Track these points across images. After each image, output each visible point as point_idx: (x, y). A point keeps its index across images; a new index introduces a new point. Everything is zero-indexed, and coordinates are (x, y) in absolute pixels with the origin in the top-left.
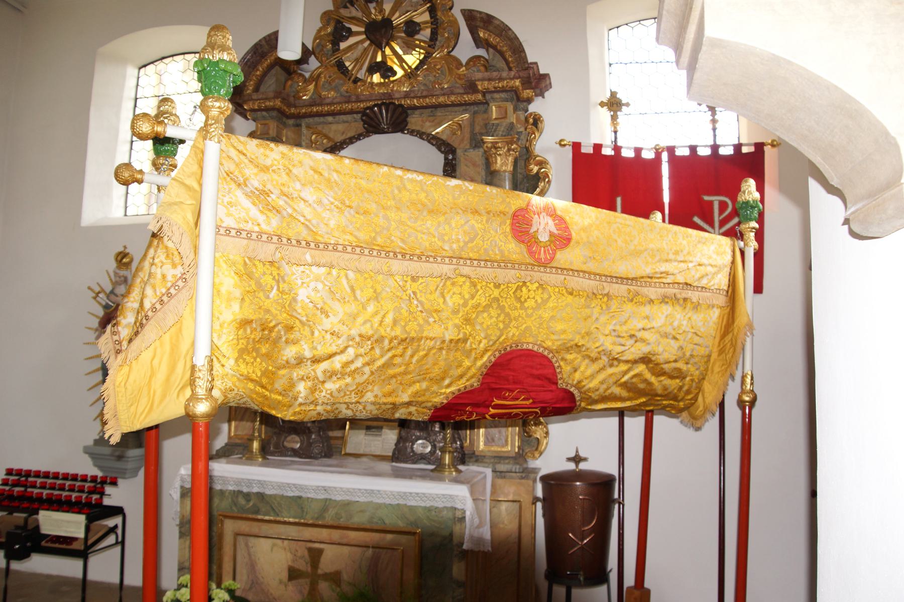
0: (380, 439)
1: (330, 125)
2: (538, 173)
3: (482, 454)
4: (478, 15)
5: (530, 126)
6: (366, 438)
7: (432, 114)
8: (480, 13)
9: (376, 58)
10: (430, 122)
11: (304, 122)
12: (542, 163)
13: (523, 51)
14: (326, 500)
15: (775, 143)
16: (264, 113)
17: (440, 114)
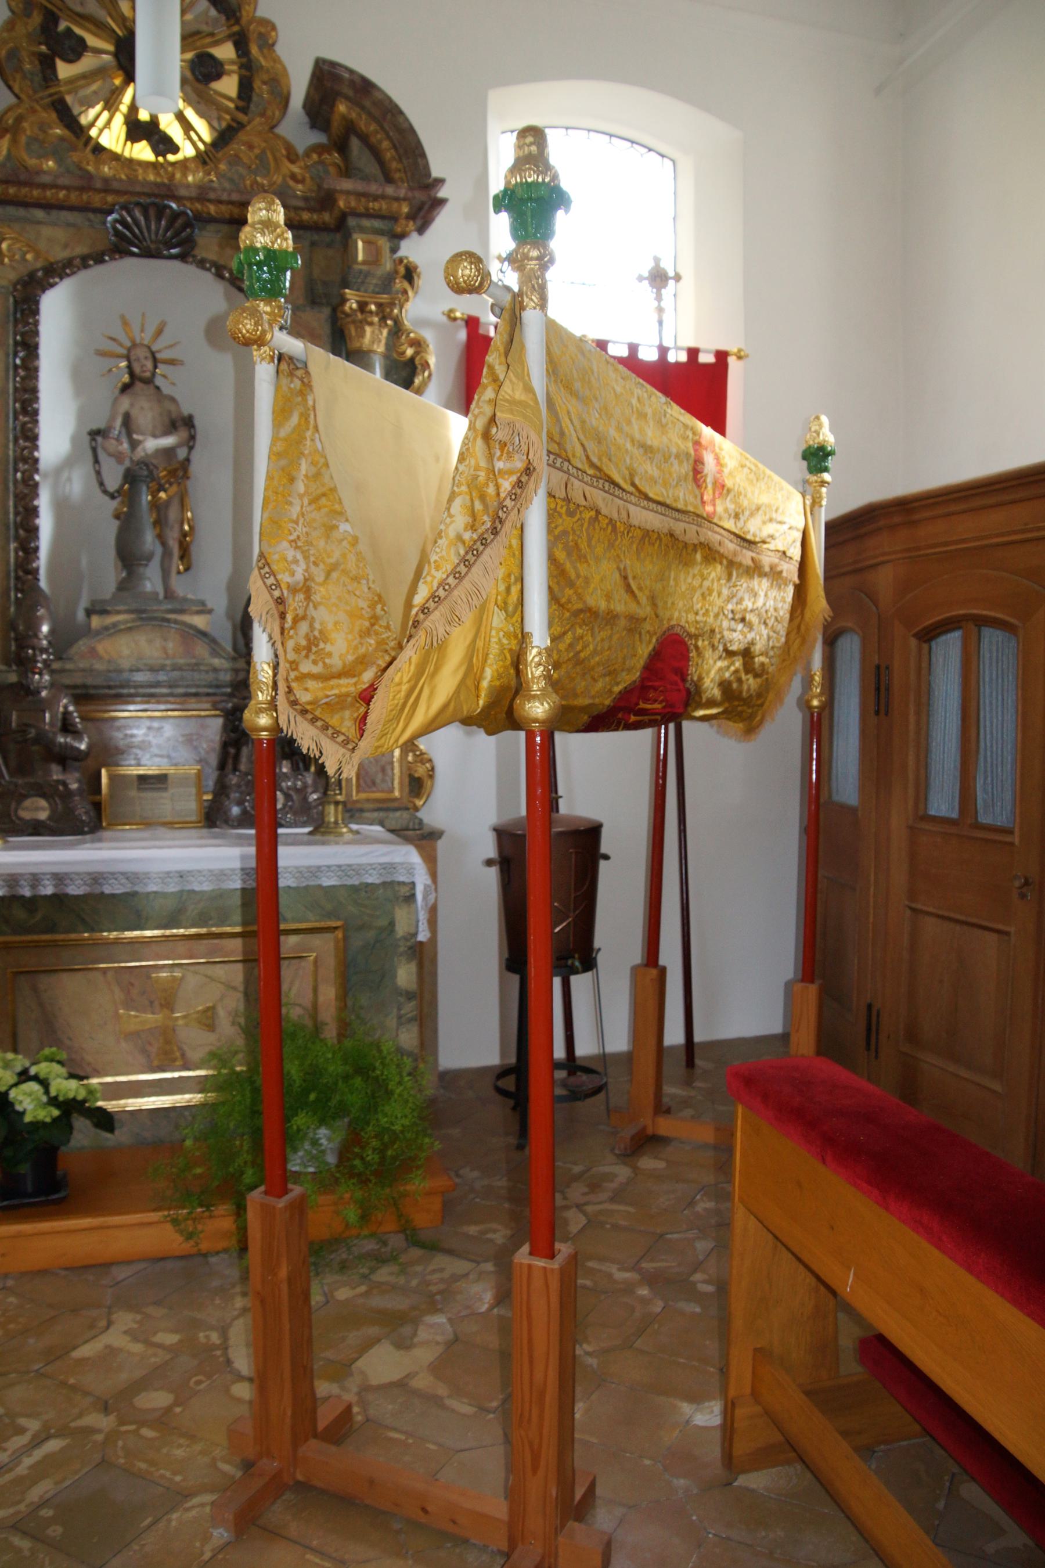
0: (165, 794)
2: (412, 359)
3: (358, 806)
8: (351, 72)
12: (418, 344)
13: (423, 155)
14: (182, 892)
15: (742, 353)
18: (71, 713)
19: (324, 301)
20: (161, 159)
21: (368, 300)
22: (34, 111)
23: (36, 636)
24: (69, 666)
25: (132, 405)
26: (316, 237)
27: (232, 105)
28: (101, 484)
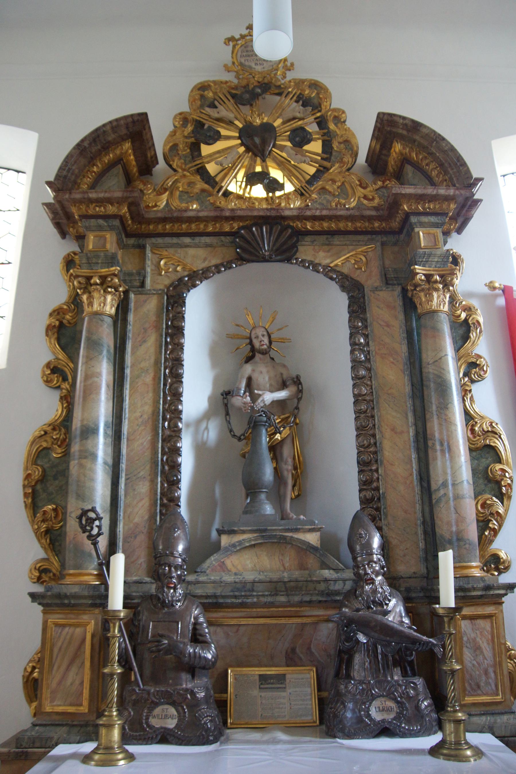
0: (283, 694)
1: (187, 249)
2: (466, 320)
4: (401, 121)
5: (449, 265)
6: (263, 694)
7: (327, 242)
8: (404, 118)
9: (254, 168)
10: (324, 251)
11: (149, 244)
13: (464, 164)
16: (101, 222)
17: (338, 243)
18: (201, 624)
19: (395, 282)
20: (271, 194)
21: (432, 273)
22: (184, 176)
23: (172, 554)
24: (202, 578)
25: (253, 370)
26: (385, 239)
27: (319, 158)
28: (231, 431)
